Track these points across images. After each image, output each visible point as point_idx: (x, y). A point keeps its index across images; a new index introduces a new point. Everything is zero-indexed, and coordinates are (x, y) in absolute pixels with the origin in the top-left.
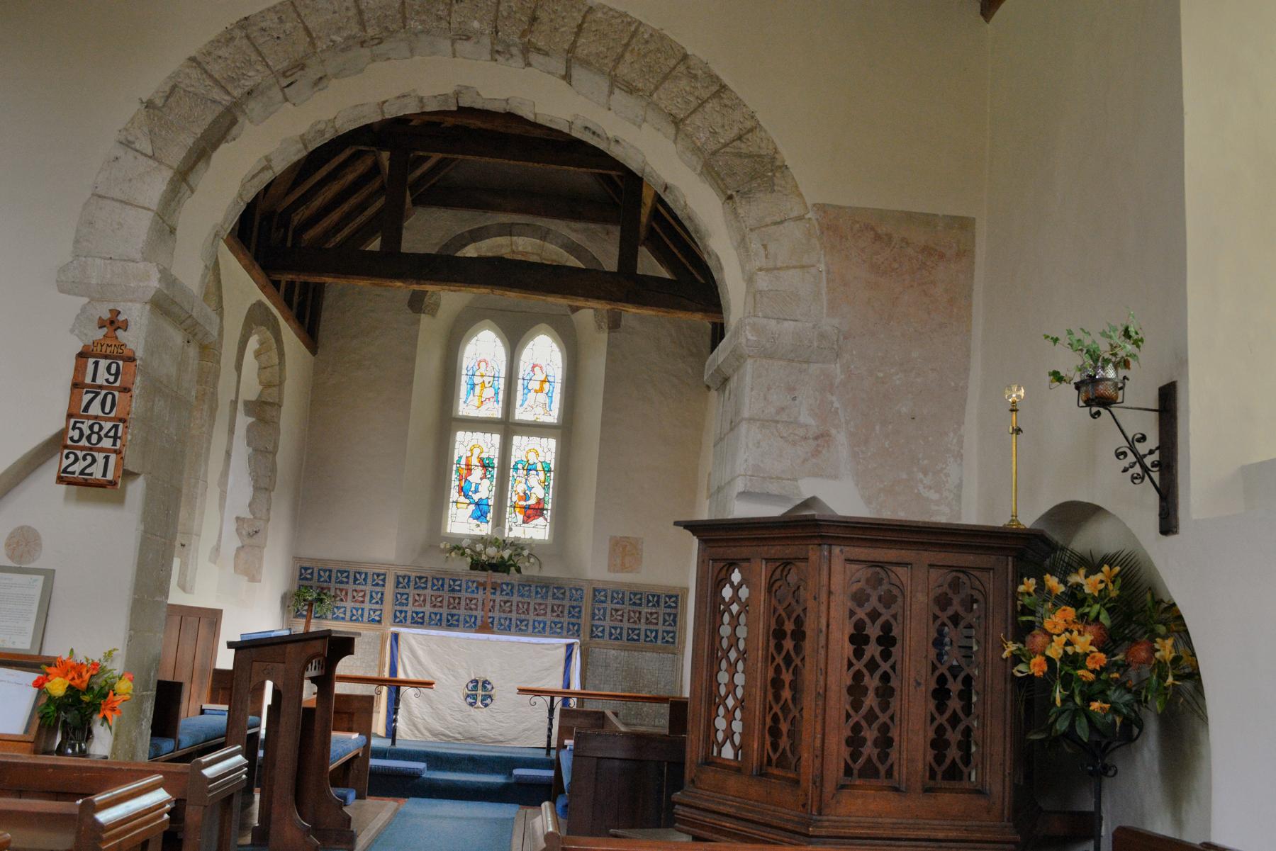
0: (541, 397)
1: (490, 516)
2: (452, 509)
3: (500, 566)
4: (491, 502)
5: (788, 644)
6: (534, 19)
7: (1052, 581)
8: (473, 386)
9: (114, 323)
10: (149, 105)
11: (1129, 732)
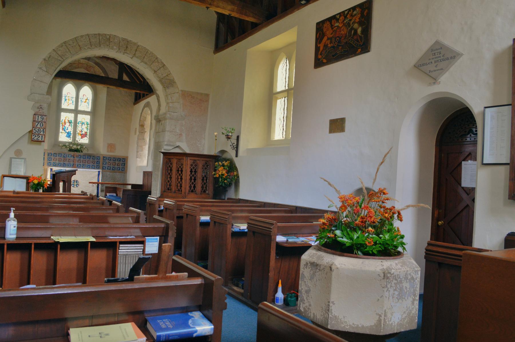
0: (86, 104)
1: (71, 136)
2: (60, 134)
3: (76, 150)
4: (72, 132)
5: (180, 172)
6: (127, 47)
7: (220, 163)
8: (66, 100)
9: (41, 108)
10: (45, 59)
11: (230, 185)
